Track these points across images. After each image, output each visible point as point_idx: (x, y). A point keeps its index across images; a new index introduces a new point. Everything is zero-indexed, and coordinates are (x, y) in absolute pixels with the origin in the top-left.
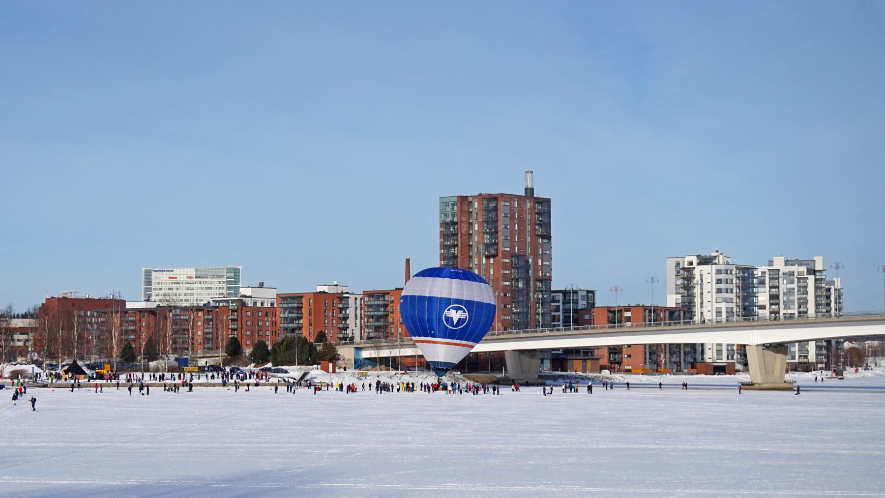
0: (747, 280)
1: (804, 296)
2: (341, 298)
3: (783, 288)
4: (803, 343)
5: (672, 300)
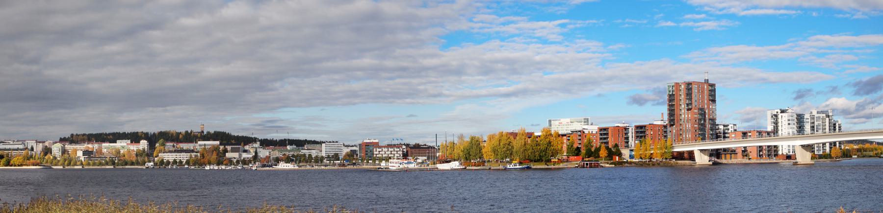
0: (800, 119)
1: (631, 134)
2: (626, 129)
3: (816, 123)
4: (824, 144)
5: (770, 128)
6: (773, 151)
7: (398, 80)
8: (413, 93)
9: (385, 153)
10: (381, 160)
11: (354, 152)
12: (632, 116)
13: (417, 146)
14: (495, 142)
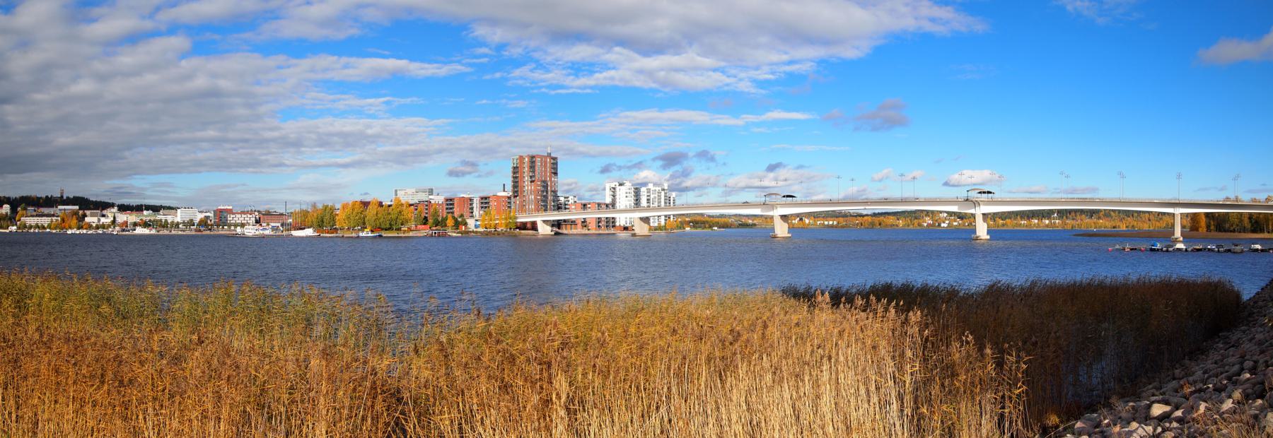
1: (476, 204)
2: (471, 200)
5: (608, 200)
6: (611, 223)
7: (241, 151)
8: (255, 164)
9: (239, 219)
10: (236, 225)
11: (207, 217)
12: (470, 187)
13: (268, 214)
14: (348, 210)
